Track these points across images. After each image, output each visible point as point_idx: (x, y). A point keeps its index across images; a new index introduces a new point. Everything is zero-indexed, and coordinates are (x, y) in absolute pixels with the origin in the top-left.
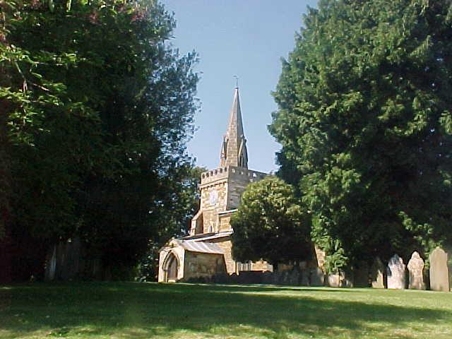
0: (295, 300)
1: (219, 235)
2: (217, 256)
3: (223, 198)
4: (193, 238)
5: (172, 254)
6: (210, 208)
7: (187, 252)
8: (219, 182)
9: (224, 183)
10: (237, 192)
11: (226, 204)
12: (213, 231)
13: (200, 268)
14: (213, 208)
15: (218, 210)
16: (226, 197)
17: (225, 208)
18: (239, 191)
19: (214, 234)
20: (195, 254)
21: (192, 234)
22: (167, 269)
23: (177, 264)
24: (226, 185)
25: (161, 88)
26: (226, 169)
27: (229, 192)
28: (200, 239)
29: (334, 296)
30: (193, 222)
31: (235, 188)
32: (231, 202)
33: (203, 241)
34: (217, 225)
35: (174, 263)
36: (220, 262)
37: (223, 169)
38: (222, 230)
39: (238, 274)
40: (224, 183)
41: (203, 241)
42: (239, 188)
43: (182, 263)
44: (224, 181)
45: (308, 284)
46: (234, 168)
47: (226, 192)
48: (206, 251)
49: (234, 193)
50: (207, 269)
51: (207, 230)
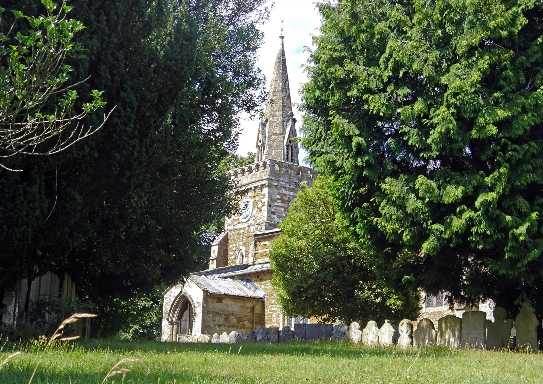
0: (35, 374)
1: (257, 268)
2: (254, 302)
3: (260, 210)
4: (214, 272)
5: (184, 296)
6: (239, 226)
7: (208, 296)
8: (253, 186)
9: (262, 186)
10: (283, 201)
11: (265, 219)
12: (245, 262)
13: (227, 319)
14: (245, 225)
15: (252, 229)
16: (265, 208)
17: (264, 228)
18: (285, 198)
19: (246, 266)
20: (220, 298)
21: (213, 266)
22: (174, 320)
23: (192, 315)
24: (266, 190)
25: (277, 167)
26: (265, 164)
27: (272, 200)
28: (226, 274)
29: (71, 320)
30: (213, 248)
31: (279, 194)
32: (273, 216)
33: (226, 278)
34: (251, 252)
35: (186, 313)
36: (258, 310)
37: (261, 164)
38: (259, 261)
39: (293, 329)
40: (262, 186)
41: (232, 277)
42: (285, 195)
43: (199, 311)
44: (263, 183)
45: (14, 157)
46: (279, 164)
47: (265, 200)
48: (245, 295)
49: (279, 203)
50: (238, 321)
51: (235, 260)
